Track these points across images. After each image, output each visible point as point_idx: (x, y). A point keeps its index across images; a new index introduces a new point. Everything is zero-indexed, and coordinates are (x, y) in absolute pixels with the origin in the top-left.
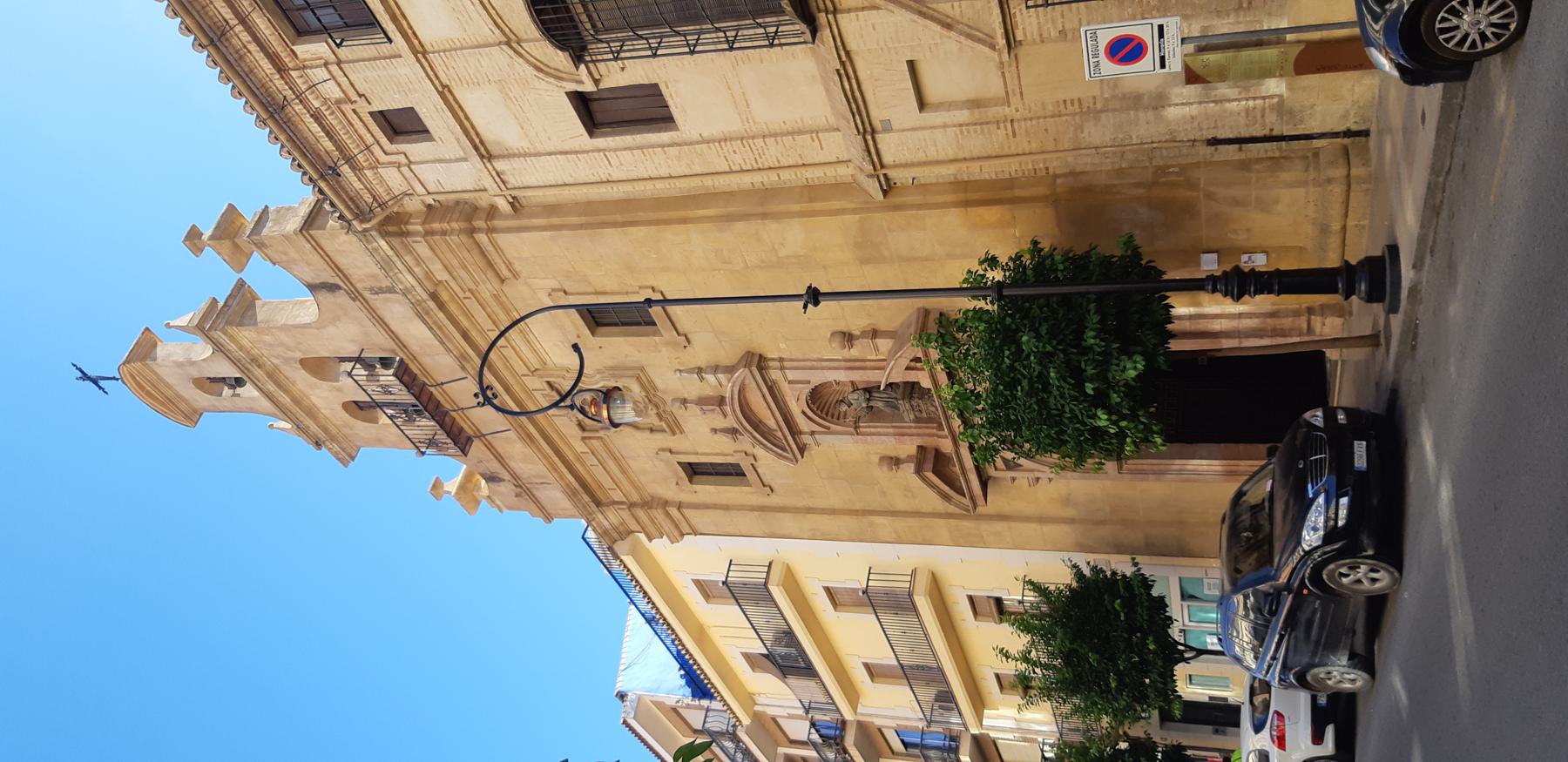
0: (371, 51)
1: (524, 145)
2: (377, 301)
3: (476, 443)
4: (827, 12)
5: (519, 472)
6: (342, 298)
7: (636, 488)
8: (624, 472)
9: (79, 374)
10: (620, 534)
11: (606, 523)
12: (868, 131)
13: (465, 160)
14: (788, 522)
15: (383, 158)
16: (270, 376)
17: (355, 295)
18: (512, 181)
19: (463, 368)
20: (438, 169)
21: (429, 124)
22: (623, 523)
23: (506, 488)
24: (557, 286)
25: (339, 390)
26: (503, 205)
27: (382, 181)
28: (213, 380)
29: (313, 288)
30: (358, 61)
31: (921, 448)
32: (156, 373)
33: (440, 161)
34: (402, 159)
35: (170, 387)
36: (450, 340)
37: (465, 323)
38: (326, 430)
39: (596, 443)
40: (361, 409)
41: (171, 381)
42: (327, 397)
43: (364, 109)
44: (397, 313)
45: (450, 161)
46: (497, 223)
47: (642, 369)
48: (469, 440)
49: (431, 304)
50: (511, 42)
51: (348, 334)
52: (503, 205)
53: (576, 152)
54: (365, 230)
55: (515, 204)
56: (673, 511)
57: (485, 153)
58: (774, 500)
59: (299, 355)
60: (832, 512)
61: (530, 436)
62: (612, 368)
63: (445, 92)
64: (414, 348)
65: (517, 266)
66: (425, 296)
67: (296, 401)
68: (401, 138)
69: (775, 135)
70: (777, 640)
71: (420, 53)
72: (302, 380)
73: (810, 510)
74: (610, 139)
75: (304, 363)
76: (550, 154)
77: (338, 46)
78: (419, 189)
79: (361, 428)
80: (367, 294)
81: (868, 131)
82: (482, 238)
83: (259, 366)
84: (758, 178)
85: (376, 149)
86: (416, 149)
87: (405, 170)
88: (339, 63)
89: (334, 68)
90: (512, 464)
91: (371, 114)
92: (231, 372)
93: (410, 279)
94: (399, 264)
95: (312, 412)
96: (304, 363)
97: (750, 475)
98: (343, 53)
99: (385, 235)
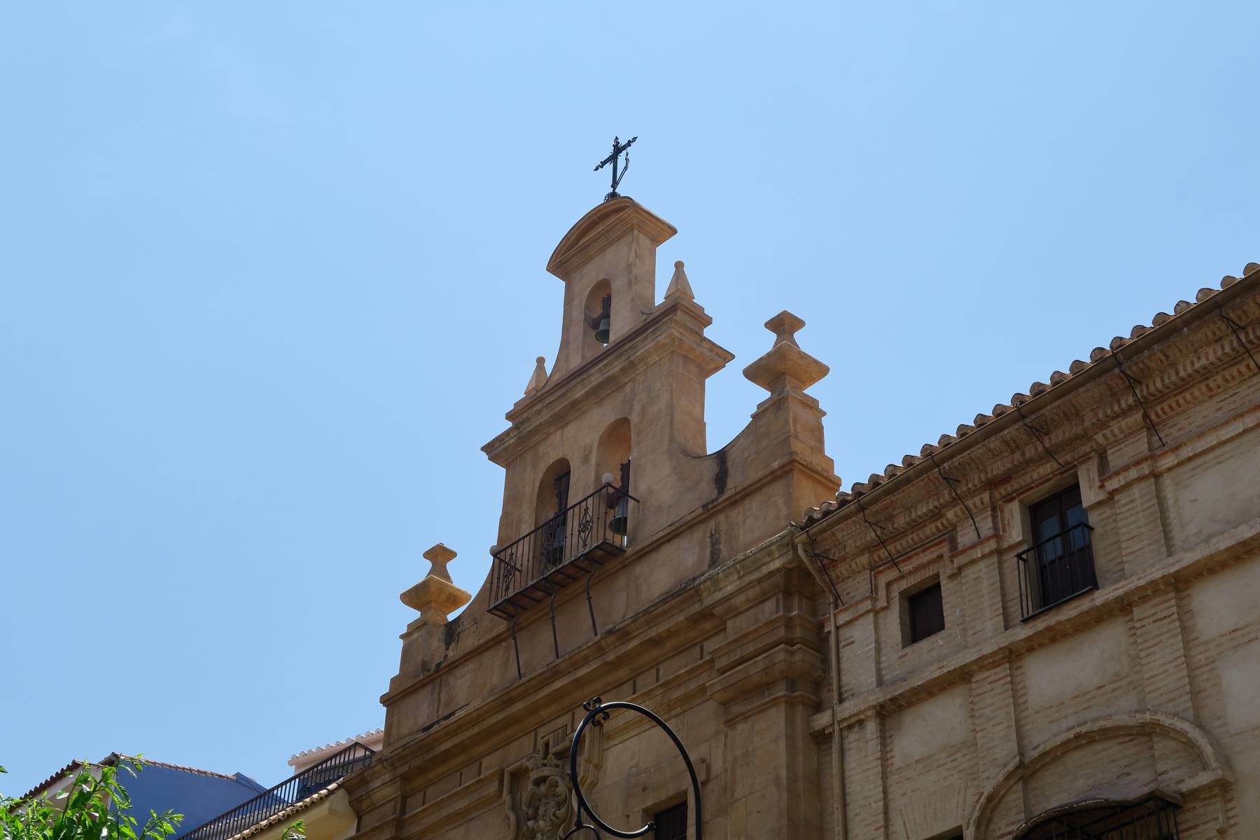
0: (1013, 592)
1: (897, 761)
2: (700, 535)
3: (502, 626)
4: (1152, 457)
5: (459, 672)
6: (707, 490)
9: (623, 142)
10: (360, 800)
11: (377, 783)
13: (880, 683)
15: (883, 580)
16: (610, 380)
17: (710, 511)
18: (852, 737)
19: (610, 632)
20: (867, 648)
24: (714, 772)
25: (586, 460)
26: (823, 719)
28: (607, 302)
30: (1001, 573)
33: (878, 650)
34: (882, 603)
35: (602, 250)
37: (670, 644)
38: (533, 433)
39: (493, 788)
40: (560, 476)
41: (609, 255)
42: (579, 442)
43: (945, 570)
44: (686, 556)
45: (878, 662)
48: (509, 617)
49: (696, 608)
50: (1026, 771)
51: (660, 489)
53: (886, 826)
54: (795, 548)
55: (821, 739)
57: (889, 712)
59: (634, 418)
61: (510, 702)
63: (963, 676)
64: (639, 569)
65: (741, 727)
66: (707, 602)
67: (575, 405)
68: (906, 604)
71: (1012, 656)
72: (599, 418)
75: (623, 423)
76: (885, 792)
77: (1019, 556)
78: (843, 618)
79: (533, 478)
80: (712, 524)
82: (780, 691)
83: (623, 369)
85: (892, 574)
86: (893, 624)
87: (868, 605)
88: (1000, 552)
89: (992, 545)
90: (471, 666)
91: (937, 575)
92: (621, 324)
93: (731, 588)
94: (748, 579)
95: (560, 420)
96: (623, 423)
98: (1011, 560)
99: (787, 571)
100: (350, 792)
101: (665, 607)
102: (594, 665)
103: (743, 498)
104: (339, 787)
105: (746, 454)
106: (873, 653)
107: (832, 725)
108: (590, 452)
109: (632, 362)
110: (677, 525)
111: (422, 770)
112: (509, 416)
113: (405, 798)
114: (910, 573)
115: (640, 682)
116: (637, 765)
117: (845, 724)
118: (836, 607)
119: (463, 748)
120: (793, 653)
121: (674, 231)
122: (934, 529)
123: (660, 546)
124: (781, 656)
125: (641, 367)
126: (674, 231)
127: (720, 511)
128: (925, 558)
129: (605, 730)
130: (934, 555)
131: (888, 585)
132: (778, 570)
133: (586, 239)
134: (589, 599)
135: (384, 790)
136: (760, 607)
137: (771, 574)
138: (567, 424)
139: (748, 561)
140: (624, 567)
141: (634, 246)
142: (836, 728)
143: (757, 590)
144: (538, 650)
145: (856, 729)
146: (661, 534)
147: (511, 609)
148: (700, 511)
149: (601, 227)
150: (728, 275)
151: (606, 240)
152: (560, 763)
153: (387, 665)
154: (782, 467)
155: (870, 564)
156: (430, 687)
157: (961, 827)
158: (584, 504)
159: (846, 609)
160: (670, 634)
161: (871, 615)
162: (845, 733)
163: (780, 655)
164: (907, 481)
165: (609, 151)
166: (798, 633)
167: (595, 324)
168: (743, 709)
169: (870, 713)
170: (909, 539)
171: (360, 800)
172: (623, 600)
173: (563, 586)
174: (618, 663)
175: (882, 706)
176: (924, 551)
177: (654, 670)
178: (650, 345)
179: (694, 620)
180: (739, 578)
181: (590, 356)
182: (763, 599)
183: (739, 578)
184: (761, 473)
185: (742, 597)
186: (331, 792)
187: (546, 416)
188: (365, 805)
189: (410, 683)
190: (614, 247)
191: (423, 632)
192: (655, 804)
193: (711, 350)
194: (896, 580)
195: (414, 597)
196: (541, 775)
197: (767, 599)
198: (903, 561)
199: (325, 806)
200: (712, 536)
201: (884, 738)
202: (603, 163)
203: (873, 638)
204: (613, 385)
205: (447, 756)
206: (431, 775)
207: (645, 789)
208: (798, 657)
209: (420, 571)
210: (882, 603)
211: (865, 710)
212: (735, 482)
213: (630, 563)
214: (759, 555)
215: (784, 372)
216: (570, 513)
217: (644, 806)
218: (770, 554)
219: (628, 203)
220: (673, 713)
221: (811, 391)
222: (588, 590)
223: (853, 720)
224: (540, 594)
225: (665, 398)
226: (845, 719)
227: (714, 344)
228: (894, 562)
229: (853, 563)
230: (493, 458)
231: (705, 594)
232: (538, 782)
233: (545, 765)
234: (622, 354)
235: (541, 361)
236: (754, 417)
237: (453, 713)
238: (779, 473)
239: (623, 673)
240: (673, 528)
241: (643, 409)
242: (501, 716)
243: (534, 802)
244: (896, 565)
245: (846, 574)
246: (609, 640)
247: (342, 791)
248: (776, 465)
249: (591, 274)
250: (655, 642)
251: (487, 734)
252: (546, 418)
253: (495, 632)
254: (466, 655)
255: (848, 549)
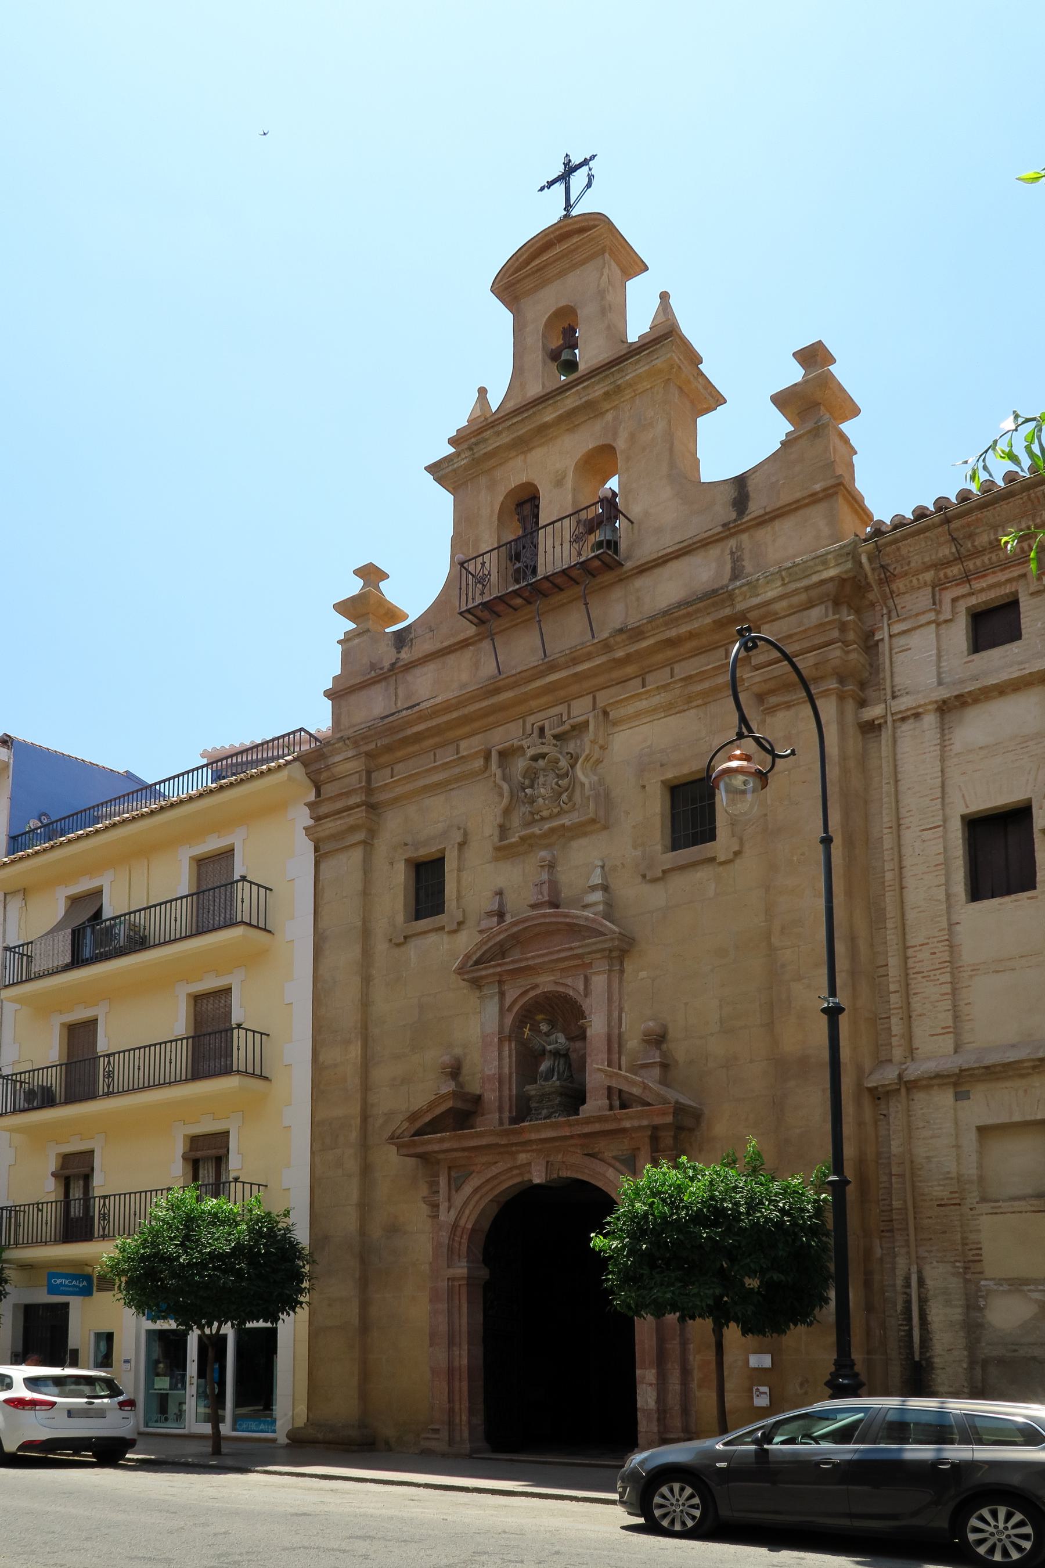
3: (471, 630)
5: (417, 671)
7: (396, 800)
8: (427, 789)
9: (576, 160)
10: (319, 772)
12: (960, 1082)
13: (940, 683)
14: (344, 957)
15: (948, 596)
17: (729, 530)
18: (906, 727)
21: (984, 654)
22: (334, 779)
23: (387, 655)
25: (559, 483)
26: (874, 712)
27: (914, 589)
29: (740, 482)
31: (478, 1099)
32: (583, 262)
33: (939, 656)
35: (562, 274)
36: (666, 624)
37: (688, 646)
39: (479, 763)
40: (525, 503)
41: (572, 279)
44: (704, 571)
45: (939, 667)
46: (850, 706)
47: (606, 828)
48: (482, 622)
49: (727, 611)
51: (654, 518)
52: (874, 712)
55: (870, 728)
56: (360, 836)
57: (951, 708)
58: (381, 946)
59: (621, 444)
60: (365, 1003)
62: (607, 795)
64: (639, 583)
66: (740, 606)
67: (543, 428)
68: (970, 620)
69: (954, 992)
70: (134, 927)
73: (367, 980)
74: (959, 834)
78: (897, 628)
80: (732, 543)
81: (960, 1082)
83: (607, 394)
84: (894, 970)
85: (964, 589)
86: (959, 633)
90: (431, 667)
92: (587, 356)
93: (770, 594)
95: (522, 445)
97: (424, 924)
99: (841, 581)
100: (305, 765)
101: (690, 609)
102: (598, 661)
103: (773, 519)
104: (295, 760)
105: (774, 479)
106: (934, 658)
107: (885, 716)
108: (564, 478)
109: (619, 387)
110: (690, 541)
111: (389, 749)
112: (452, 441)
113: (369, 773)
114: (982, 590)
115: (649, 678)
116: (650, 747)
117: (900, 716)
118: (889, 618)
119: (437, 731)
120: (847, 652)
121: (426, 468)
122: (987, 561)
123: (666, 562)
124: (838, 653)
125: (628, 394)
126: (426, 468)
127: (743, 531)
128: (1002, 577)
129: (611, 717)
130: (1016, 574)
131: (954, 600)
132: (832, 579)
133: (545, 257)
134: (586, 604)
135: (347, 765)
136: (805, 613)
137: (822, 582)
138: (530, 450)
139: (796, 569)
140: (621, 580)
141: (606, 271)
142: (889, 719)
143: (803, 597)
144: (521, 649)
145: (911, 721)
146: (670, 550)
147: (485, 615)
148: (720, 529)
149: (558, 249)
150: (727, 311)
151: (563, 267)
152: (558, 743)
153: (330, 665)
154: (824, 490)
155: (933, 582)
156: (384, 684)
157: (1030, 800)
158: (558, 525)
159: (904, 620)
160: (691, 635)
161: (934, 625)
162: (898, 724)
163: (835, 653)
164: (1005, 496)
165: (560, 169)
166: (851, 636)
167: (554, 356)
168: (787, 698)
169: (930, 707)
170: (986, 559)
171: (319, 772)
172: (618, 609)
173: (546, 596)
174: (628, 659)
175: (944, 702)
176: (1002, 570)
177: (668, 669)
178: (642, 369)
179: (721, 624)
180: (783, 585)
181: (551, 386)
182: (810, 605)
183: (783, 585)
184: (798, 495)
185: (784, 603)
186: (288, 763)
187: (505, 438)
188: (323, 776)
189: (358, 680)
190: (578, 272)
191: (365, 637)
192: (675, 777)
193: (706, 389)
194: (963, 596)
195: (346, 608)
196: (539, 751)
197: (813, 607)
198: (976, 579)
199: (283, 774)
200: (732, 553)
201: (943, 729)
202: (550, 184)
203: (935, 646)
204: (590, 409)
205: (418, 738)
206: (399, 754)
207: (662, 765)
208: (854, 656)
209: (355, 586)
210: (948, 616)
211: (926, 704)
212: (755, 508)
213: (628, 577)
214: (811, 563)
215: (815, 401)
216: (541, 532)
217: (663, 778)
218: (825, 563)
219: (598, 222)
220: (695, 704)
221: (846, 427)
222: (585, 596)
223: (909, 713)
224: (519, 601)
225: (661, 426)
226: (900, 712)
227: (710, 382)
228: (967, 578)
229: (914, 580)
230: (439, 480)
231: (739, 599)
232: (535, 758)
233: (543, 744)
234: (607, 376)
235: (482, 392)
236: (783, 443)
237: (418, 704)
238: (821, 495)
239: (630, 670)
240: (682, 545)
241: (632, 437)
242: (485, 704)
243: (532, 776)
244: (969, 581)
245: (903, 589)
246: (618, 639)
247: (297, 764)
248: (818, 487)
249: (546, 302)
250: (671, 643)
251: (467, 719)
252: (507, 440)
253: (461, 637)
254: (426, 656)
255: (913, 564)
